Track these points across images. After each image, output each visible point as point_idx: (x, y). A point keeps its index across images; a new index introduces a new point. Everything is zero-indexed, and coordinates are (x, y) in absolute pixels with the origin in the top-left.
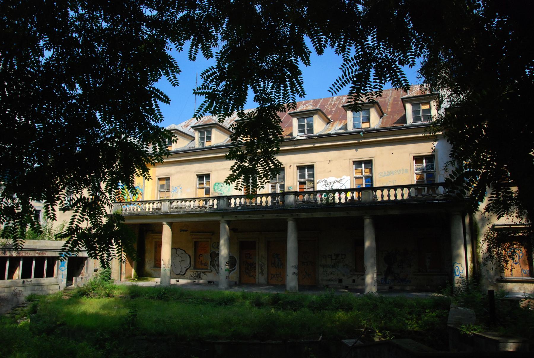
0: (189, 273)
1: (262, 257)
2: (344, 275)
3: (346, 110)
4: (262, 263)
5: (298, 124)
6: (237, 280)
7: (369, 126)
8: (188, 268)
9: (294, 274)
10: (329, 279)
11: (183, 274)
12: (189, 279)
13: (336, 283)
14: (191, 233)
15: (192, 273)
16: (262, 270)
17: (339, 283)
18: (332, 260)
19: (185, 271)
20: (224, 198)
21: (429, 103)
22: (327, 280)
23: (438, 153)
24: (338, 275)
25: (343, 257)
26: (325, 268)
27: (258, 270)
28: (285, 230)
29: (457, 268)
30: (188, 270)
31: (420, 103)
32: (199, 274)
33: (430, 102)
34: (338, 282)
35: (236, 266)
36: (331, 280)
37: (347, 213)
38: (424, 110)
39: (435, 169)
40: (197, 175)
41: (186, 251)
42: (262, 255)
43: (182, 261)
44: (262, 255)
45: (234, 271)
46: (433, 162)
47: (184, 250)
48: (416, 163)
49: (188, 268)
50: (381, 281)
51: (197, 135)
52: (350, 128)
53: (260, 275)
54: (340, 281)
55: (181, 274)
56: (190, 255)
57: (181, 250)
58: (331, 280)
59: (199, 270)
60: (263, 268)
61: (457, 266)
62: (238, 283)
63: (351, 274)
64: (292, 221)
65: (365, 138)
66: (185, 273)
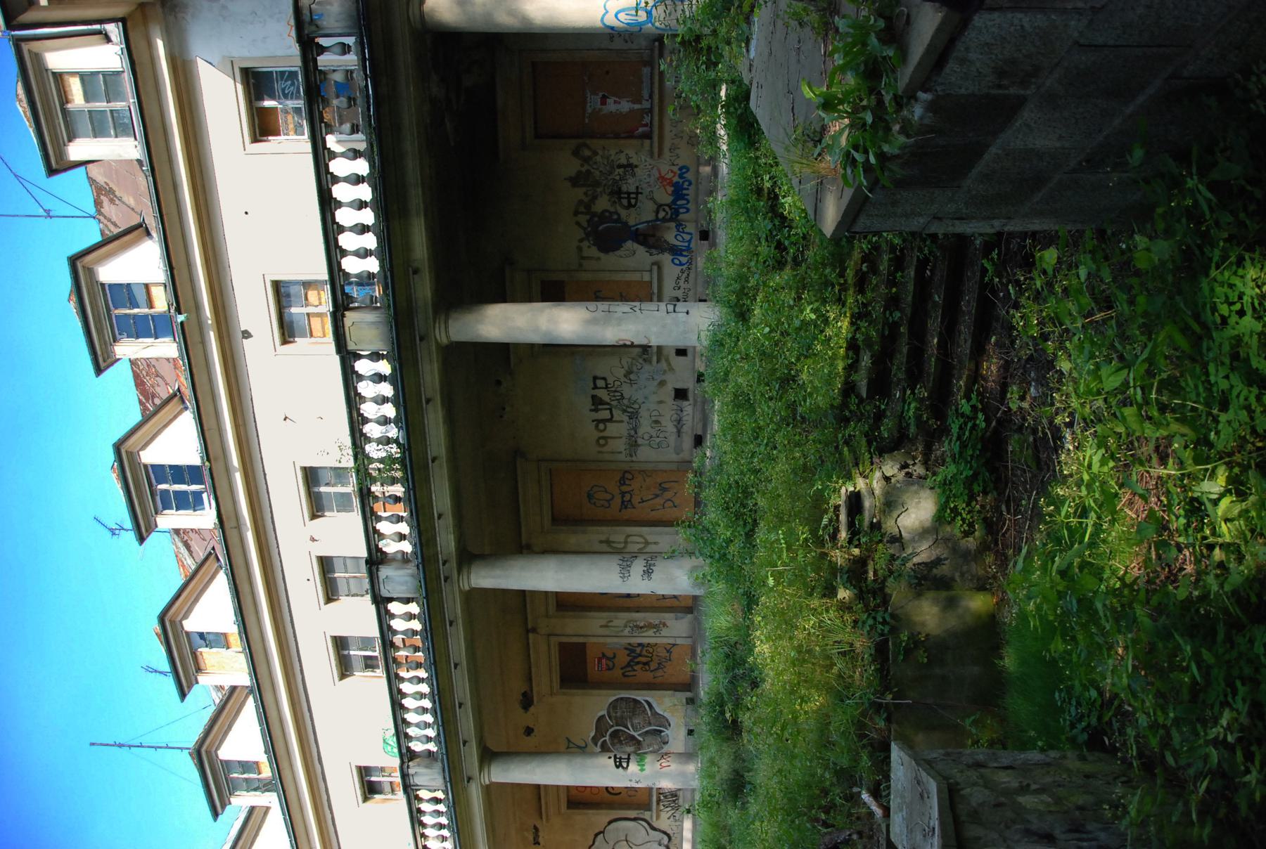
0: (664, 822)
1: (606, 626)
2: (662, 383)
3: (109, 361)
4: (626, 626)
5: (173, 512)
6: (683, 696)
7: (162, 288)
8: (649, 824)
9: (648, 572)
10: (675, 430)
11: (666, 838)
12: (682, 822)
13: (688, 407)
14: (541, 818)
15: (664, 815)
16: (650, 626)
17: (688, 400)
18: (611, 420)
19: (657, 833)
20: (408, 775)
21: (59, 77)
22: (679, 432)
23: (235, 54)
24: (661, 402)
25: (601, 383)
26: (640, 441)
27: (648, 638)
28: (502, 353)
29: (622, 16)
30: (655, 824)
31: (65, 112)
32: (665, 797)
33: (54, 74)
34: (686, 403)
35: (638, 698)
36: (679, 423)
37: (428, 401)
38: (87, 98)
39: (293, 69)
40: (365, 799)
41: (597, 831)
42: (601, 626)
43: (627, 841)
44: (601, 626)
45: (654, 705)
46: (271, 72)
47: (596, 835)
48: (278, 134)
49: (649, 824)
50: (681, 264)
51: (242, 802)
52: (129, 149)
53: (664, 632)
54: (681, 394)
55: (666, 843)
56: (608, 820)
57: (596, 843)
58: (679, 423)
59: (654, 799)
60: (642, 624)
61: (616, 16)
62: (689, 694)
63: (658, 361)
64: (469, 578)
65: (198, 307)
66: (665, 833)
